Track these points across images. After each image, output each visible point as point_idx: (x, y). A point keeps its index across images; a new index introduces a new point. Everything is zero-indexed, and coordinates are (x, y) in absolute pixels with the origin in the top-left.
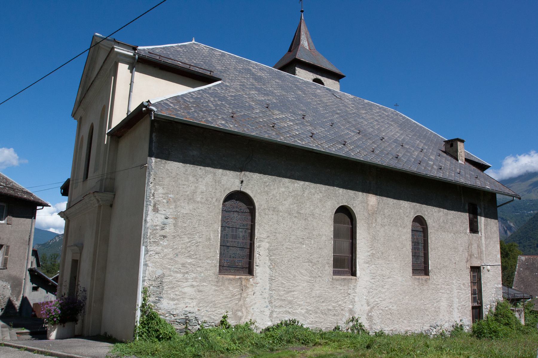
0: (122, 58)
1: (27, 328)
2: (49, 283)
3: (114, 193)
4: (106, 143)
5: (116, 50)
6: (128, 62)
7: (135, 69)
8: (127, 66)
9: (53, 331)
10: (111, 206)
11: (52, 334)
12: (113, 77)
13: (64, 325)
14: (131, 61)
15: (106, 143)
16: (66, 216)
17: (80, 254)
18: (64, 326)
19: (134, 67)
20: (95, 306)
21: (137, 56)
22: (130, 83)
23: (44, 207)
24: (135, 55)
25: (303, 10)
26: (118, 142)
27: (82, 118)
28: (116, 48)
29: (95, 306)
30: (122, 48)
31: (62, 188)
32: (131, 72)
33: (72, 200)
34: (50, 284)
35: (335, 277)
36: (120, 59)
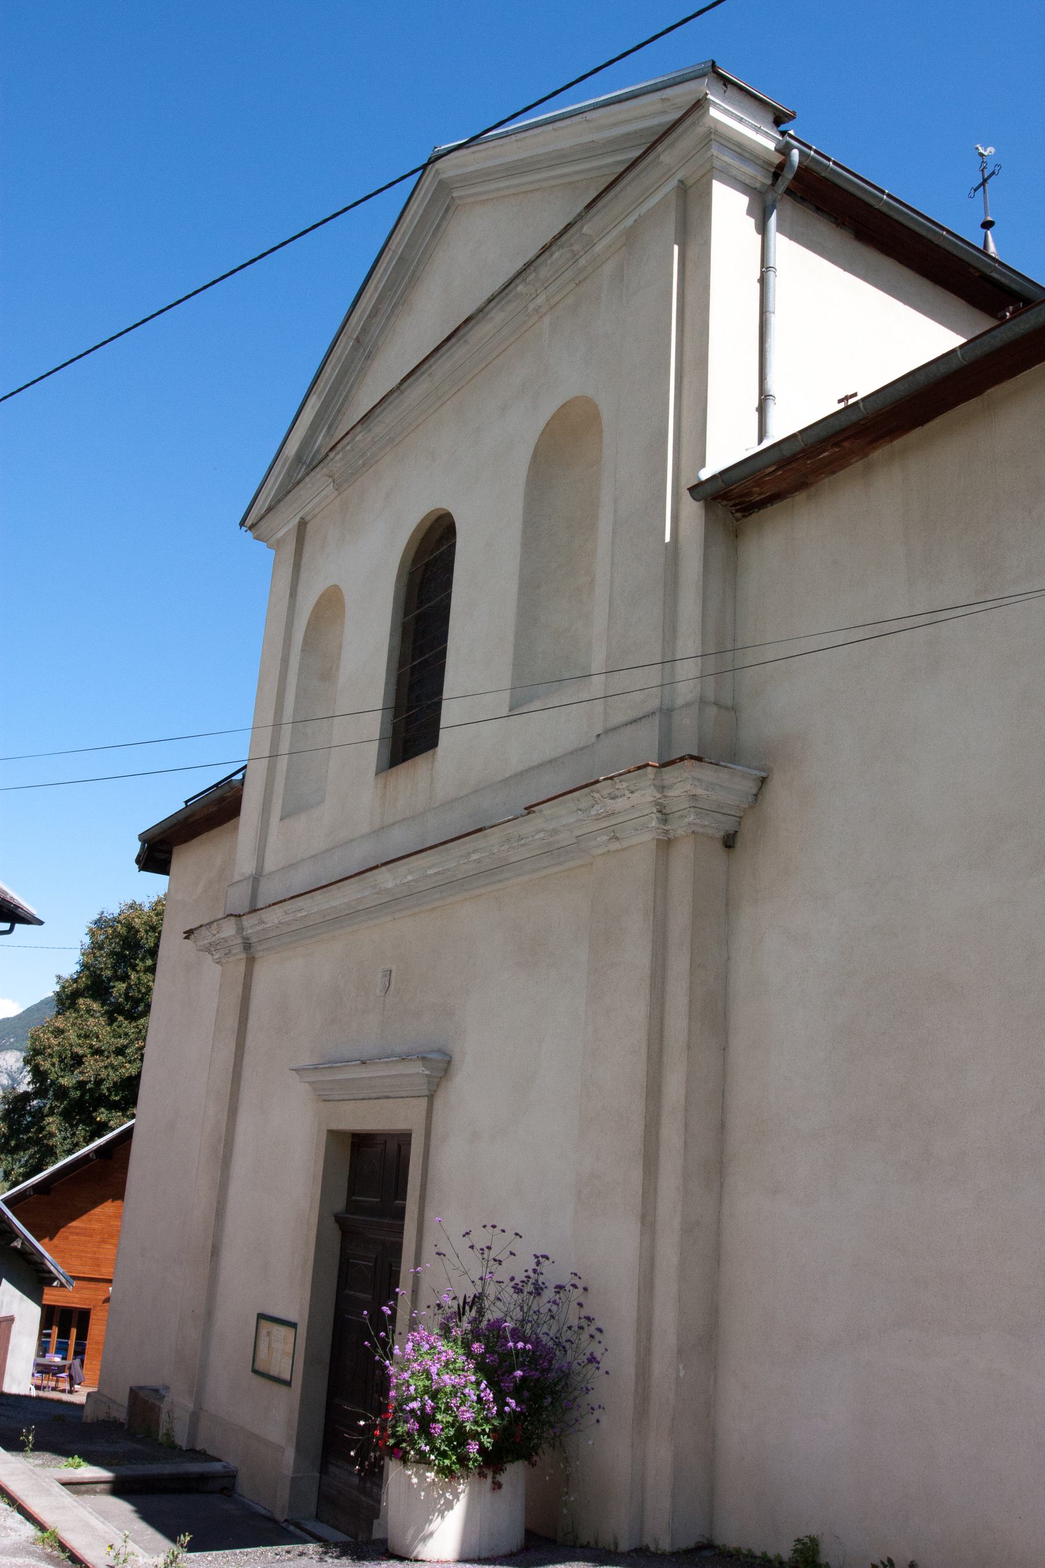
0: (727, 159)
1: (92, 1459)
2: (12, 1241)
3: (764, 774)
4: (667, 539)
5: (713, 112)
6: (747, 181)
7: (777, 213)
8: (743, 201)
9: (442, 1514)
10: (729, 842)
11: (432, 1527)
12: (676, 248)
13: (499, 1478)
14: (763, 179)
15: (667, 539)
16: (244, 938)
17: (424, 1102)
18: (497, 1486)
19: (774, 207)
20: (682, 1374)
21: (795, 153)
22: (758, 276)
23: (17, 926)
24: (784, 150)
25: (989, 218)
26: (736, 535)
27: (306, 524)
28: (715, 104)
29: (682, 1374)
30: (759, 96)
31: (145, 838)
32: (762, 229)
33: (269, 866)
34: (17, 1244)
35: (111, 1278)
36: (717, 163)
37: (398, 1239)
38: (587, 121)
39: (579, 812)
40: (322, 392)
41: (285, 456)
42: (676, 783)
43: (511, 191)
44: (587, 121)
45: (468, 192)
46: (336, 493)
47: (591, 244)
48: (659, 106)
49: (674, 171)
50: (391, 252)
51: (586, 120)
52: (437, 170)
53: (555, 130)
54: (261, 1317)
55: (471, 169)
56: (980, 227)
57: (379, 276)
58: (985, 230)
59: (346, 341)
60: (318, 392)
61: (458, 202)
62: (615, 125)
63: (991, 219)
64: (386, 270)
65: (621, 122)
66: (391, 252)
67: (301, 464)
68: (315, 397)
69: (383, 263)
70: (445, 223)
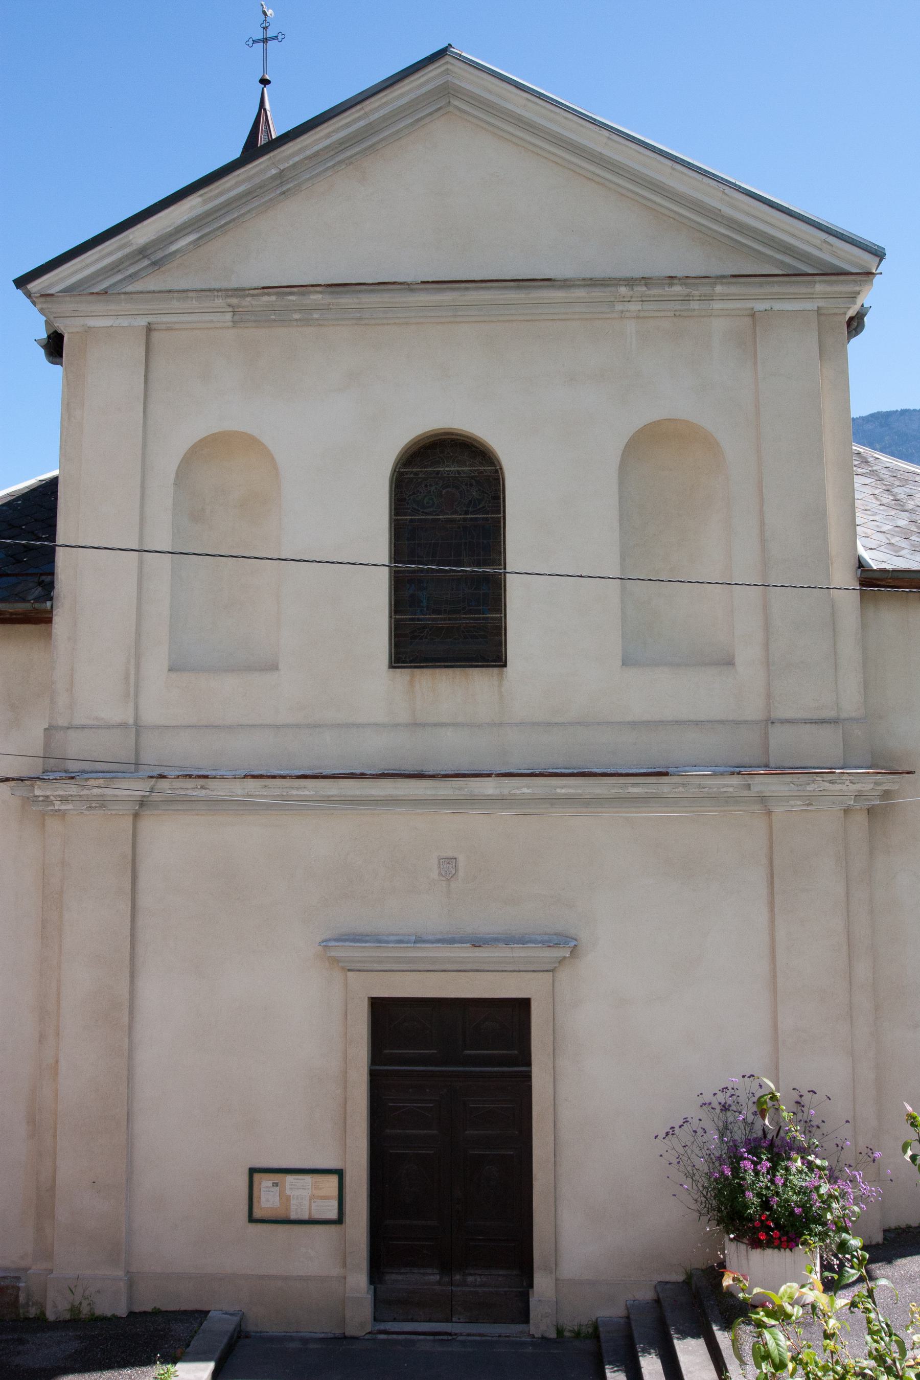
37: (529, 1083)
38: (724, 193)
39: (791, 785)
40: (211, 199)
41: (126, 240)
42: (885, 783)
43: (589, 175)
44: (724, 193)
45: (475, 113)
46: (230, 324)
47: (710, 298)
48: (818, 243)
49: (814, 296)
50: (362, 112)
51: (723, 192)
52: (448, 69)
53: (674, 169)
54: (253, 1171)
55: (510, 107)
56: (271, 83)
57: (337, 125)
58: (263, 86)
59: (267, 166)
60: (205, 197)
61: (450, 109)
62: (748, 214)
63: (268, 78)
64: (348, 125)
65: (771, 224)
66: (362, 112)
67: (141, 256)
68: (199, 200)
69: (348, 116)
70: (427, 120)
